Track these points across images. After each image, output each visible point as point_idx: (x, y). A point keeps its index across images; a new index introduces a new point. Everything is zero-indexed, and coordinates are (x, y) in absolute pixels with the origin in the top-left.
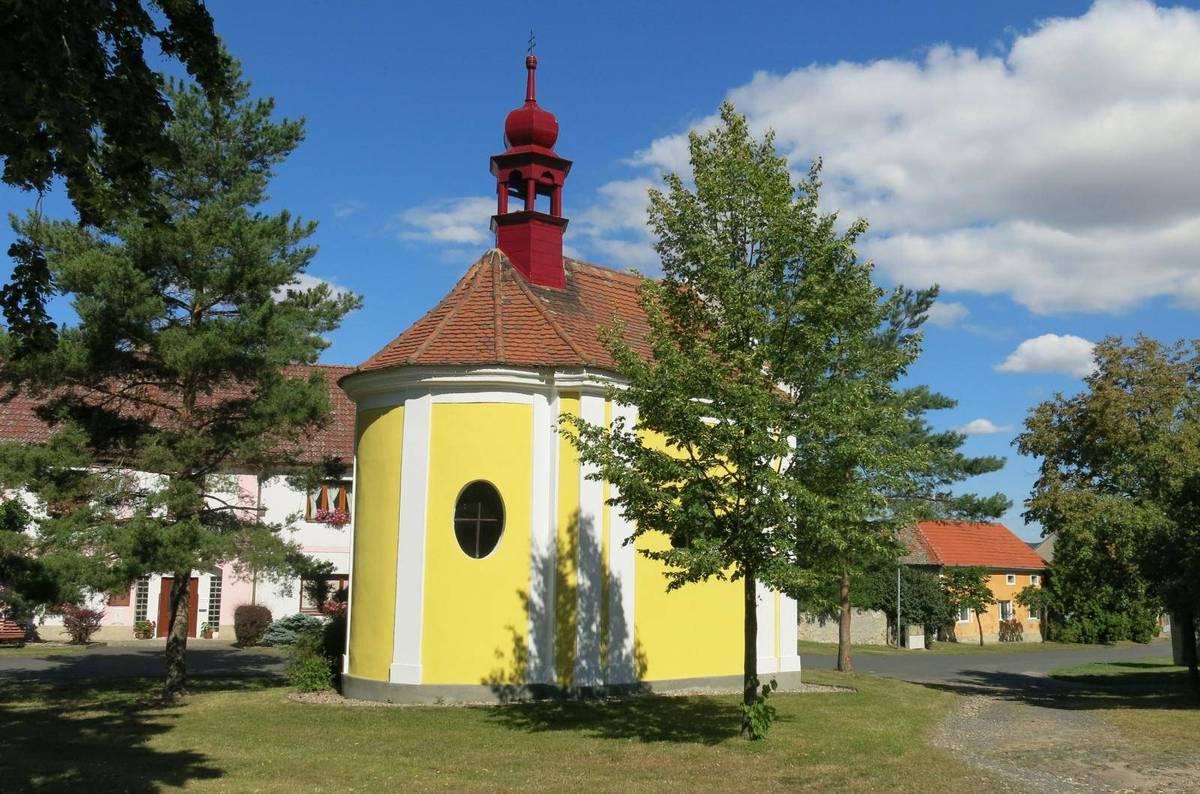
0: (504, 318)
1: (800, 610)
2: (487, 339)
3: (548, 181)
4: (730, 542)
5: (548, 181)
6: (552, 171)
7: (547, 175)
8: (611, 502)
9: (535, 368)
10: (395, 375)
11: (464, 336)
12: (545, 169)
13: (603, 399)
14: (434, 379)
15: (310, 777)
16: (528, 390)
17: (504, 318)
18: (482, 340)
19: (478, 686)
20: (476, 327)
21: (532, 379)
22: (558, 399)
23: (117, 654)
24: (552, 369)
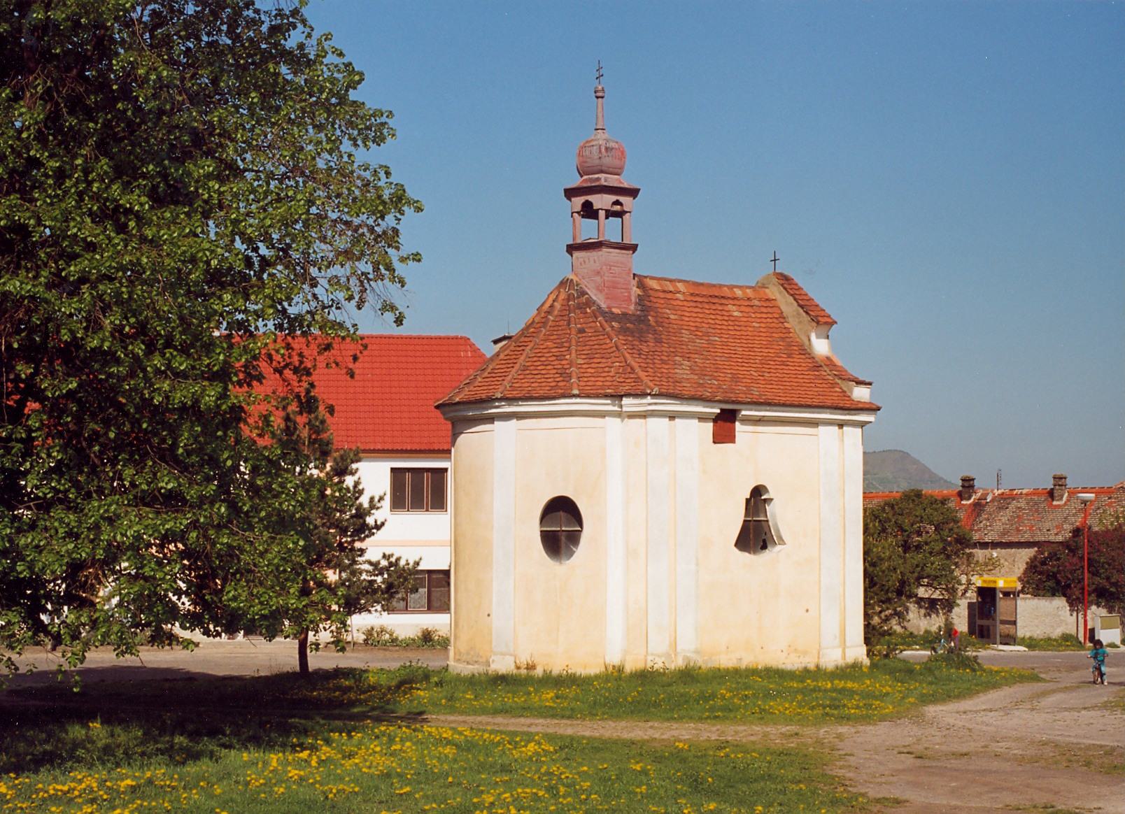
0: (579, 348)
1: (1071, 605)
2: (564, 371)
3: (618, 208)
4: (351, 565)
5: (618, 208)
6: (622, 199)
7: (617, 203)
8: (376, 522)
9: (606, 396)
10: (484, 405)
11: (543, 367)
12: (614, 198)
13: (837, 428)
14: (490, 411)
15: (737, 746)
16: (602, 415)
17: (579, 348)
18: (559, 371)
19: (849, 671)
20: (554, 358)
21: (605, 405)
22: (626, 419)
23: (248, 673)
24: (621, 397)
